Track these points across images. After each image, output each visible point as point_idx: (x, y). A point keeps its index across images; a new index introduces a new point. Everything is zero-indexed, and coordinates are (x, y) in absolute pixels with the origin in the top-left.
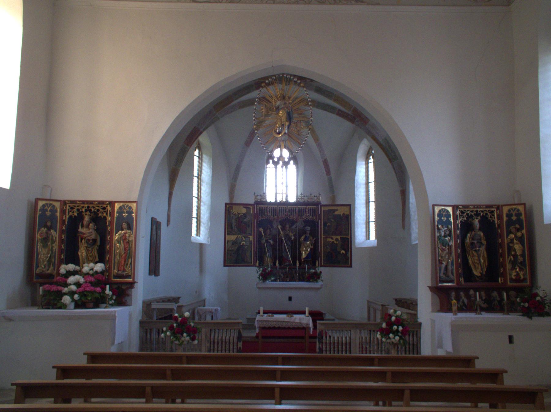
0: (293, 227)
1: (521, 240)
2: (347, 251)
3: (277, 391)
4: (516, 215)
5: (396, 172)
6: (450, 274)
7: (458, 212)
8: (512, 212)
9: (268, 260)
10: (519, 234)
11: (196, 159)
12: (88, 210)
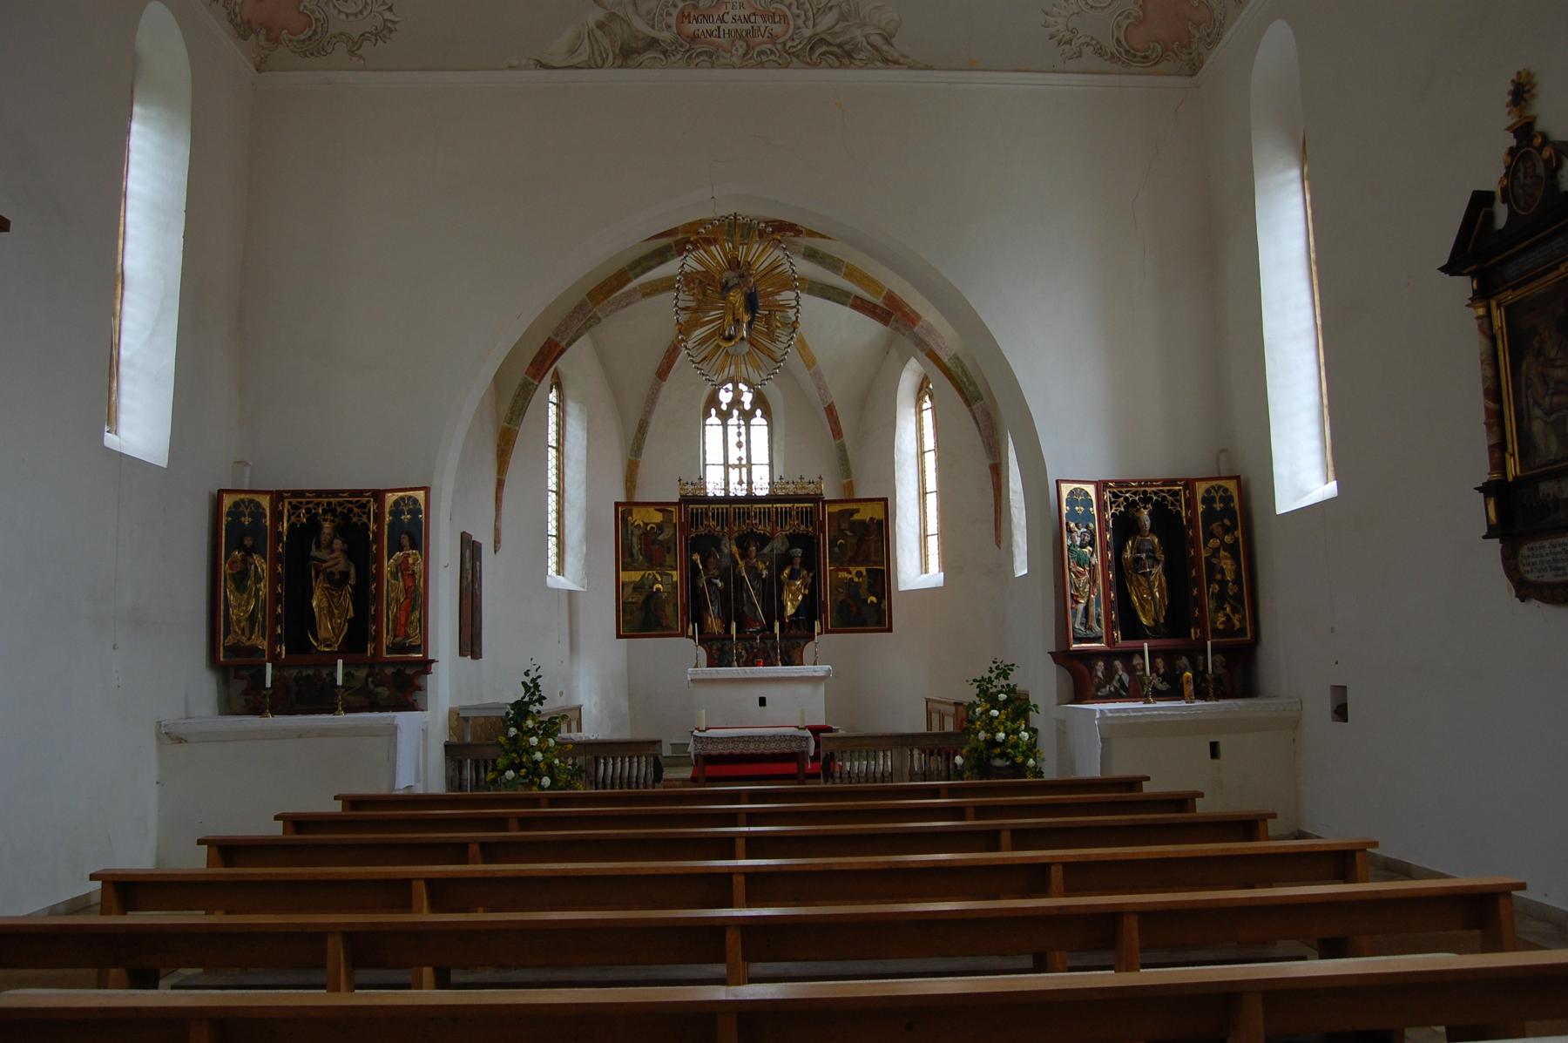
0: (766, 550)
1: (1233, 549)
2: (880, 597)
3: (739, 881)
4: (1222, 499)
5: (983, 415)
6: (1095, 625)
7: (1107, 496)
8: (242, 508)
9: (714, 624)
10: (1227, 539)
11: (552, 418)
12: (330, 509)
